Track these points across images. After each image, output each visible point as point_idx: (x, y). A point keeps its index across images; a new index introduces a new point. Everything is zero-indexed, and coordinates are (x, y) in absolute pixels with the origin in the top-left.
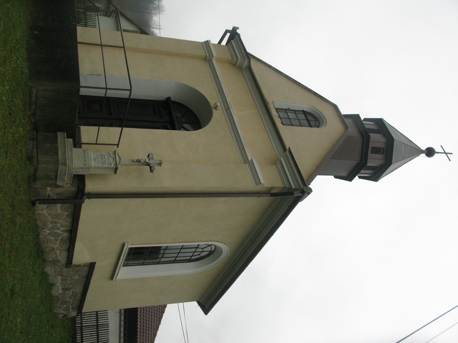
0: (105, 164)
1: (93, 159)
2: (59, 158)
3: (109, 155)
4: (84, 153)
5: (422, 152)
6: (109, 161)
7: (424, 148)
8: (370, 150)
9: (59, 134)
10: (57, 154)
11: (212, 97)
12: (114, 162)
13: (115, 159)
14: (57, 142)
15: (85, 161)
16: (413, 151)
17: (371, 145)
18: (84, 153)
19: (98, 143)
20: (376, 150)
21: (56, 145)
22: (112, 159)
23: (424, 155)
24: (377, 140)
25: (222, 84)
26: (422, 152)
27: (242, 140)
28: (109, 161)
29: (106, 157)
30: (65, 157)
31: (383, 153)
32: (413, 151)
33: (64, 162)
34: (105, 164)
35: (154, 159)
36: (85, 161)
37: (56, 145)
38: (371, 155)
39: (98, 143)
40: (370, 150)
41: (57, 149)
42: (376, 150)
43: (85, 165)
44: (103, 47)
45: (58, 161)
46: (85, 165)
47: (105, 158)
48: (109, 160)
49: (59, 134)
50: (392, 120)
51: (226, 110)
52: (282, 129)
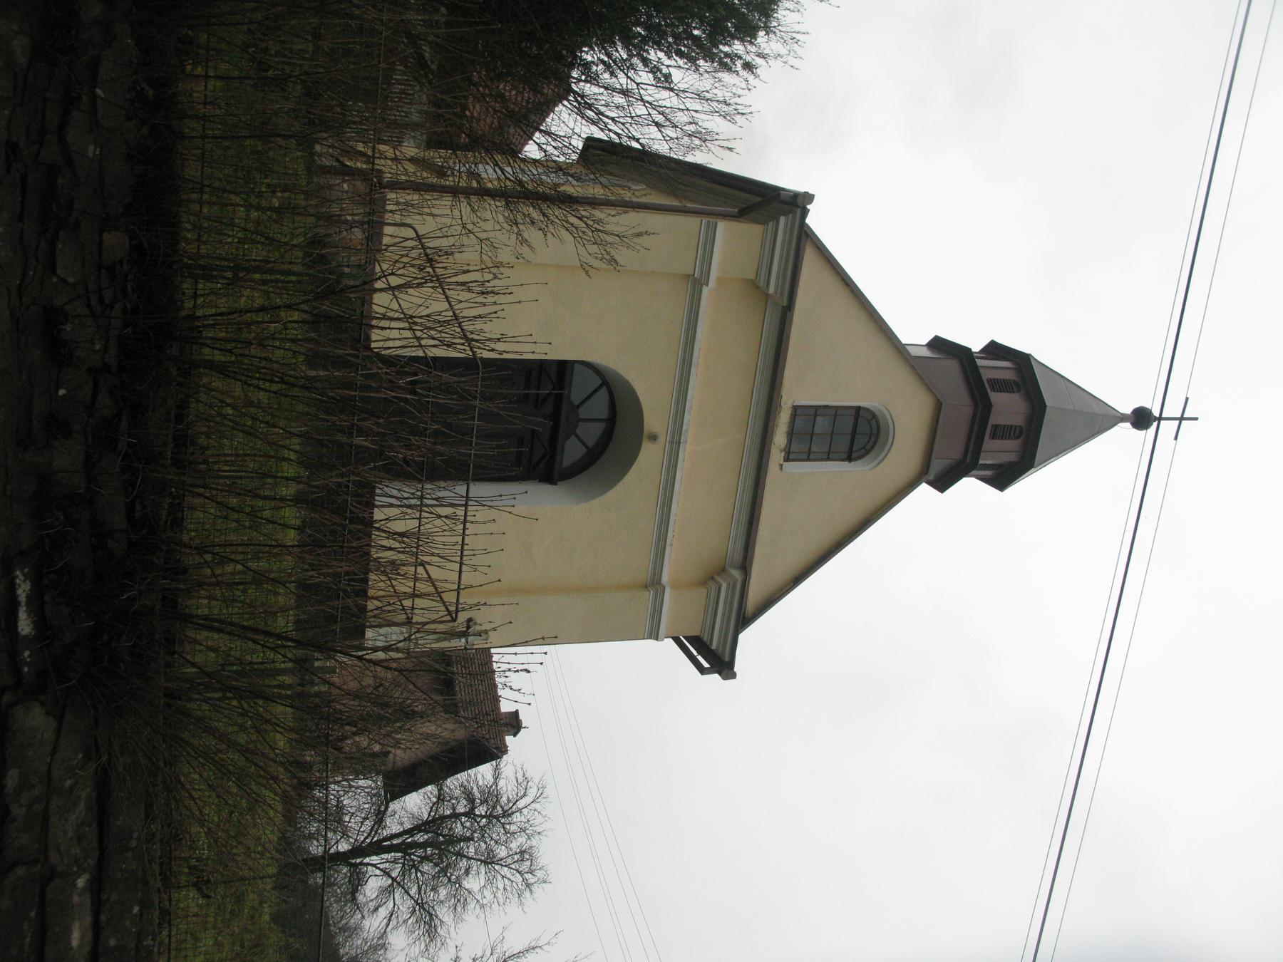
5: (1123, 418)
7: (1127, 409)
8: (997, 415)
11: (654, 417)
16: (1094, 419)
17: (995, 419)
20: (1002, 432)
23: (1128, 425)
24: (1008, 408)
25: (693, 372)
26: (1123, 418)
27: (670, 529)
31: (1017, 438)
32: (1094, 419)
33: (761, 284)
38: (989, 444)
40: (997, 415)
42: (1002, 432)
50: (1050, 352)
51: (672, 443)
52: (776, 456)
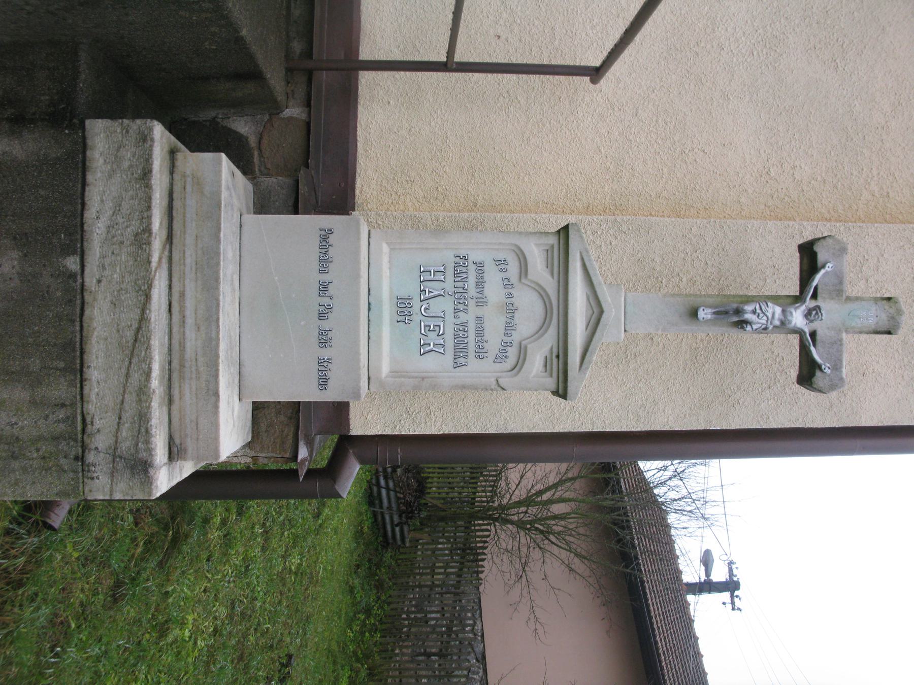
0: (481, 353)
1: (387, 311)
2: (91, 408)
3: (513, 268)
4: (324, 262)
6: (509, 327)
9: (102, 135)
10: (77, 371)
12: (549, 340)
13: (557, 312)
14: (75, 238)
15: (324, 340)
18: (324, 262)
19: (458, 58)
21: (72, 263)
22: (538, 308)
28: (509, 327)
29: (494, 291)
30: (143, 392)
33: (125, 446)
34: (481, 353)
35: (851, 290)
36: (324, 340)
37: (72, 263)
39: (458, 58)
41: (75, 297)
43: (323, 382)
44: (547, 555)
45: (78, 433)
46: (323, 382)
47: (481, 302)
48: (510, 310)
49: (102, 135)
